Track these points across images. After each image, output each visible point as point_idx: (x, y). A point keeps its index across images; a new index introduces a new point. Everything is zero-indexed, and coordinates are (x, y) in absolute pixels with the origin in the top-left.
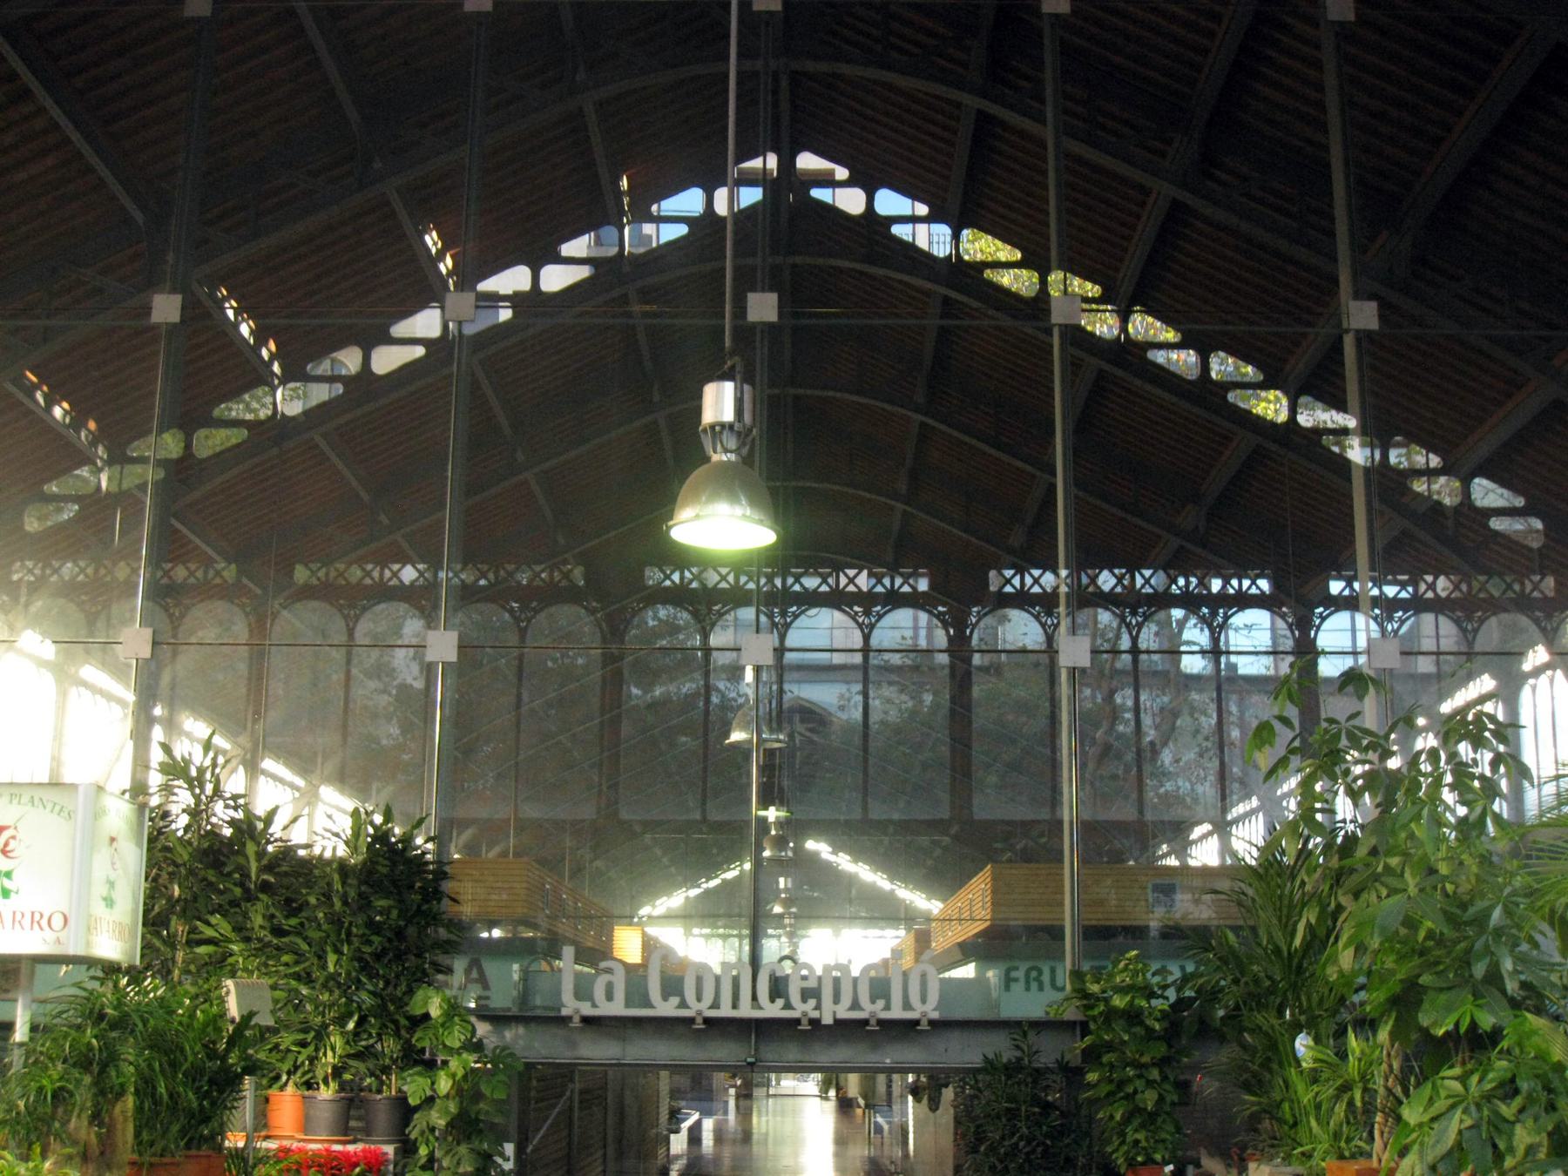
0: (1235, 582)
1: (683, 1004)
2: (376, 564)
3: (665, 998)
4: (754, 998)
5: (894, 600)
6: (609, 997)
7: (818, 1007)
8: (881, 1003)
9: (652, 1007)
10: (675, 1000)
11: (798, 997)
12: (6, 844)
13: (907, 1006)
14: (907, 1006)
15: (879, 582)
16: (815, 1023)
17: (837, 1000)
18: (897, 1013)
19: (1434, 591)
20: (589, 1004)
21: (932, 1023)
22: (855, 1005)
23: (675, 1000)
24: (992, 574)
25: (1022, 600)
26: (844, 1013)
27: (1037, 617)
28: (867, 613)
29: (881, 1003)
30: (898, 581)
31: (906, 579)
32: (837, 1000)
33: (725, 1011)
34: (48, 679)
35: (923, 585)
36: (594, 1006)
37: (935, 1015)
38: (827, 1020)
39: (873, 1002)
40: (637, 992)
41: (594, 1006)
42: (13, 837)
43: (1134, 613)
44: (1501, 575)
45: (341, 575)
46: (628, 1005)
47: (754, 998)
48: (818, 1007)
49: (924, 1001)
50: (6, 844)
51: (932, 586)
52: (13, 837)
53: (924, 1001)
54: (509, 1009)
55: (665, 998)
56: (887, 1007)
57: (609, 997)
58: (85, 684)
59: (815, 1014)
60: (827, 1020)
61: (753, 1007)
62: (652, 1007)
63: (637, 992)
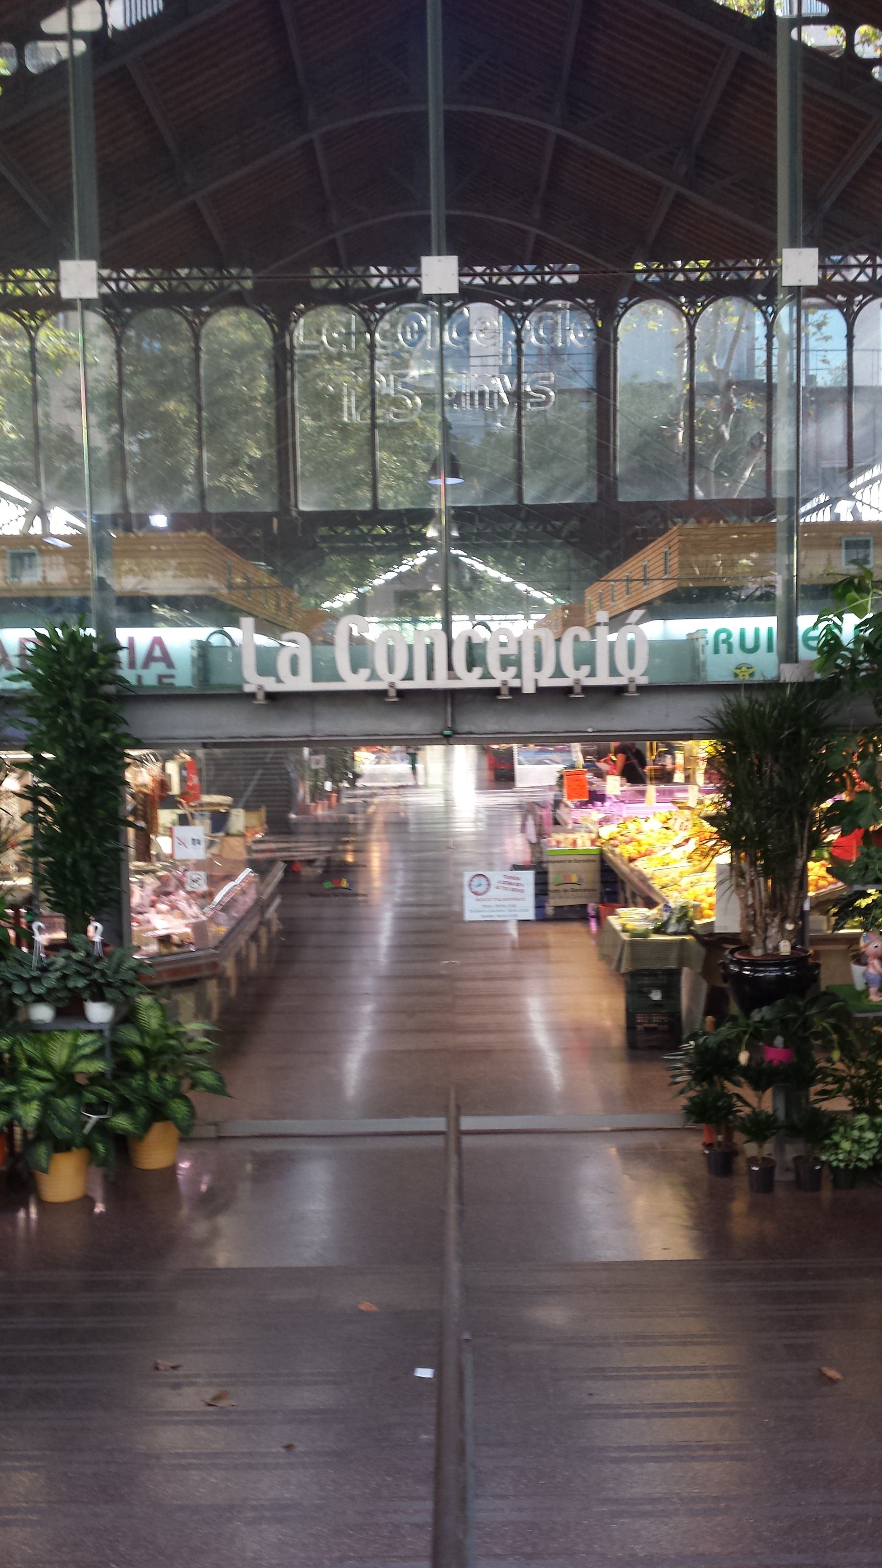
3: (355, 670)
4: (450, 667)
6: (295, 671)
7: (519, 676)
13: (614, 671)
14: (614, 671)
16: (516, 691)
17: (538, 666)
18: (603, 679)
20: (272, 679)
21: (641, 689)
22: (559, 672)
26: (546, 682)
32: (538, 666)
37: (643, 681)
38: (529, 688)
39: (577, 668)
41: (279, 681)
46: (315, 679)
47: (450, 667)
49: (631, 665)
55: (355, 670)
56: (592, 674)
57: (295, 671)
59: (515, 683)
60: (529, 688)
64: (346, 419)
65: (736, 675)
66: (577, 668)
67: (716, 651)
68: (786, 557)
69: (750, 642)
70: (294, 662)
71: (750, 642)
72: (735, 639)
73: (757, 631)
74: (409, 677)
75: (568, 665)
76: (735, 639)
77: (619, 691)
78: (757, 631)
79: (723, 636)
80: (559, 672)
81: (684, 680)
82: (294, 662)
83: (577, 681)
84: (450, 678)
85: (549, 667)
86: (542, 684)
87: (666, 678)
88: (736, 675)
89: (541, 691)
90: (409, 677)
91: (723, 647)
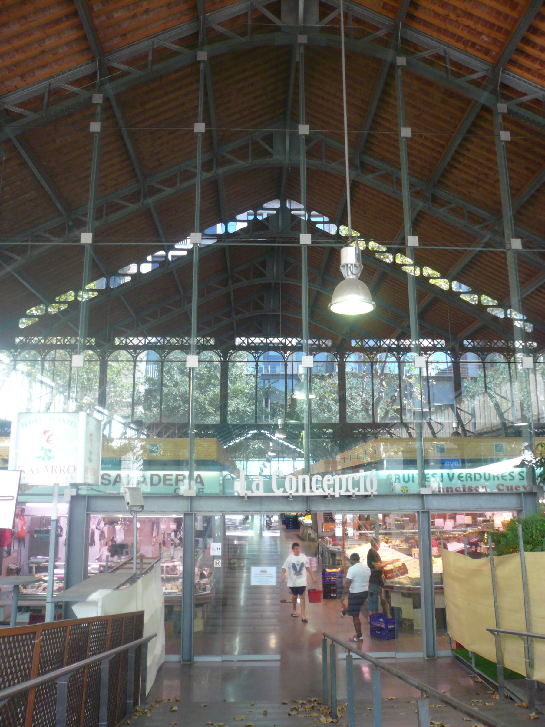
0: (269, 341)
1: (285, 491)
2: (265, 338)
3: (278, 489)
4: (311, 488)
5: (434, 349)
6: (258, 489)
7: (334, 491)
8: (356, 489)
9: (274, 492)
10: (282, 490)
11: (327, 487)
12: (48, 438)
13: (366, 490)
14: (366, 490)
15: (530, 344)
16: (333, 496)
17: (340, 488)
18: (362, 493)
19: (291, 343)
20: (250, 492)
21: (375, 496)
22: (347, 490)
23: (282, 490)
24: (116, 339)
25: (126, 347)
26: (343, 493)
27: (252, 354)
28: (135, 352)
29: (356, 489)
30: (317, 343)
31: (262, 342)
32: (340, 488)
33: (300, 493)
34: (26, 380)
35: (212, 342)
36: (252, 492)
37: (376, 493)
38: (337, 496)
39: (354, 489)
40: (268, 488)
41: (252, 492)
42: (51, 435)
43: (257, 353)
44: (483, 340)
45: (131, 341)
46: (265, 491)
47: (311, 488)
48: (334, 491)
49: (372, 488)
50: (48, 438)
51: (215, 342)
52: (51, 435)
53: (372, 488)
54: (219, 494)
55: (278, 489)
56: (359, 491)
57: (258, 489)
58: (286, 383)
59: (333, 494)
60: (337, 496)
61: (310, 492)
62: (274, 492)
63: (268, 488)
64: (238, 341)
65: (402, 491)
66: (354, 489)
67: (467, 480)
68: (419, 443)
69: (406, 479)
70: (258, 485)
71: (406, 479)
72: (401, 478)
73: (408, 476)
74: (297, 491)
75: (350, 488)
76: (401, 478)
77: (366, 496)
78: (408, 476)
79: (469, 475)
80: (347, 490)
81: (388, 493)
82: (258, 485)
83: (354, 493)
84: (310, 492)
85: (344, 488)
86: (342, 494)
87: (383, 492)
88: (402, 491)
89: (341, 496)
90: (297, 491)
91: (469, 479)
